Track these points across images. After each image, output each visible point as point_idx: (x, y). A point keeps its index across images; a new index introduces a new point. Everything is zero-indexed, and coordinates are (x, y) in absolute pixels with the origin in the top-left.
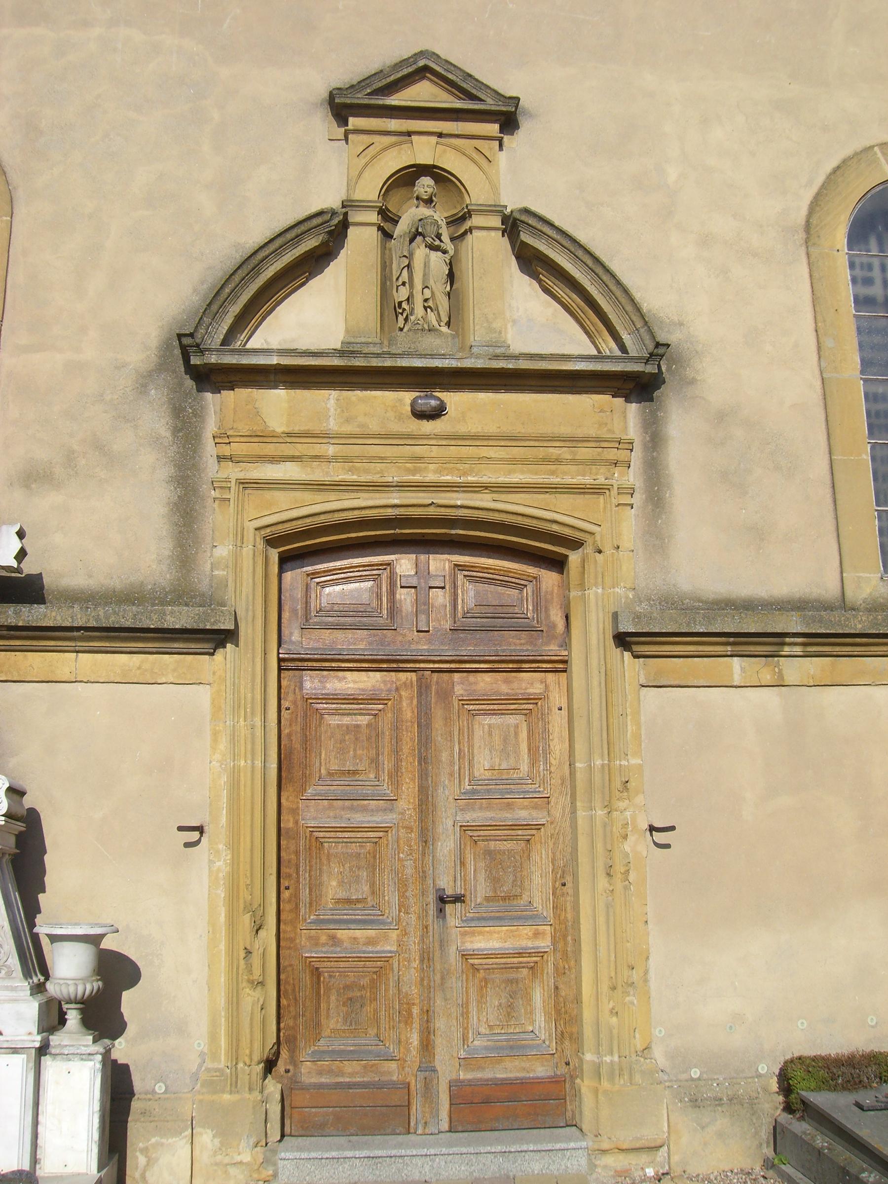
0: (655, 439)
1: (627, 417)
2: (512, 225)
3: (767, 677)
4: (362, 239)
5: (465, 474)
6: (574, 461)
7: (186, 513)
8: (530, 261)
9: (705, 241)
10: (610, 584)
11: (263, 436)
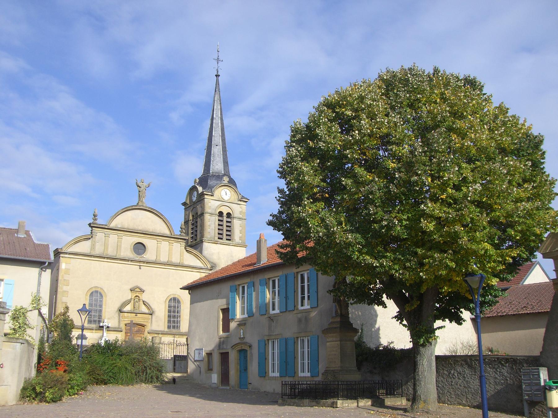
0: (152, 318)
2: (143, 301)
4: (132, 301)
7: (119, 322)
10: (147, 329)
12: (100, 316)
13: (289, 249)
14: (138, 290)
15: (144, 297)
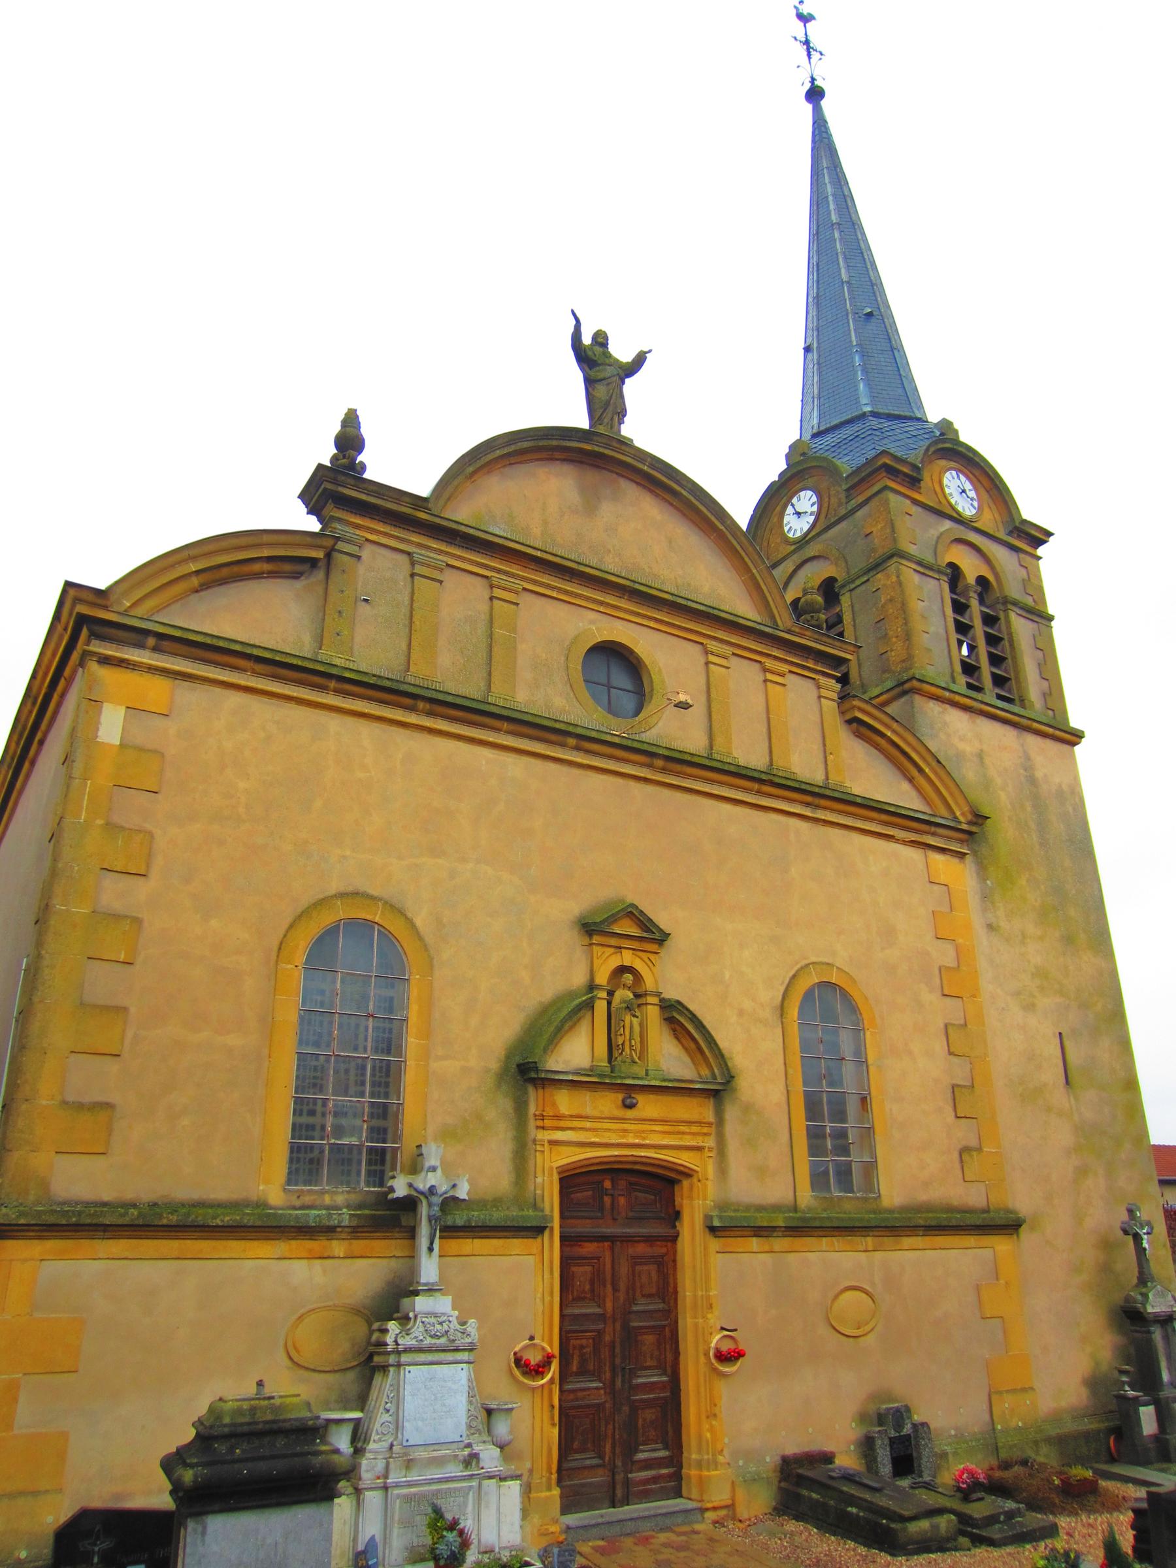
0: (720, 1121)
1: (704, 1111)
3: (767, 1248)
4: (601, 1007)
5: (644, 1139)
6: (690, 1133)
8: (670, 1021)
9: (741, 1013)
10: (696, 1206)
11: (558, 1117)
12: (384, 1119)
13: (641, 1456)
14: (628, 928)
15: (669, 976)
